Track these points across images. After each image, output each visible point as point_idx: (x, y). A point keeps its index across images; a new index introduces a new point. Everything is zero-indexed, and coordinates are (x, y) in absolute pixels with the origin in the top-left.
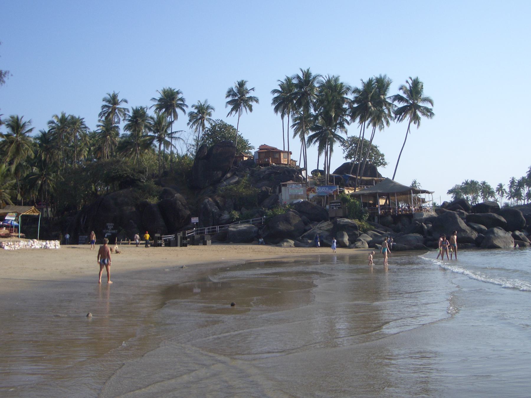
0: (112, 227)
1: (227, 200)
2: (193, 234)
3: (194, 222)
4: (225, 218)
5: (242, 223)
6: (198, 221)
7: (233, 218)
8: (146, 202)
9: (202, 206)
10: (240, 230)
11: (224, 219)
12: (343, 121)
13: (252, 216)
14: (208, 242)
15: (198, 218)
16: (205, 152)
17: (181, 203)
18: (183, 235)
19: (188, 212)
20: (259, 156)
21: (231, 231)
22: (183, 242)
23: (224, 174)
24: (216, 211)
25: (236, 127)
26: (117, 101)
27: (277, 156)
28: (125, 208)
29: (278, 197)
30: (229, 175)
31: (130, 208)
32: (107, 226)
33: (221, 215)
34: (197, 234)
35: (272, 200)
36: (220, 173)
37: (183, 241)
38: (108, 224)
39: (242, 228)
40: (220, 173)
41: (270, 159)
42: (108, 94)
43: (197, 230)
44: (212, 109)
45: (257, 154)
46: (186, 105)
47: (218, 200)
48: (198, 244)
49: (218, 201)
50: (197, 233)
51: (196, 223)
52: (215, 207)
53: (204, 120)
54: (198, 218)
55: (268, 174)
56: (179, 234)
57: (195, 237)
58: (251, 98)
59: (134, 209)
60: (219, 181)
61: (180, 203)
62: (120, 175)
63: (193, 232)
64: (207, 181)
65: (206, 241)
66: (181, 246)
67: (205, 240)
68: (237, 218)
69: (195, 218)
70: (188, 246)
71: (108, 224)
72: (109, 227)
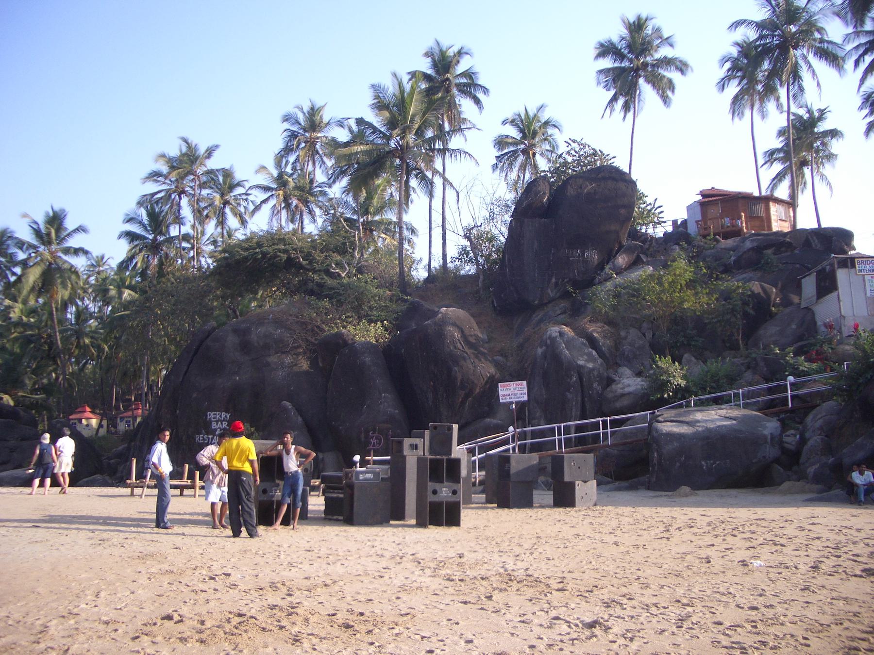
0: (225, 425)
1: (623, 334)
2: (507, 450)
3: (508, 400)
4: (627, 390)
5: (702, 404)
6: (526, 398)
7: (662, 386)
8: (339, 335)
9: (540, 351)
10: (708, 430)
11: (623, 395)
12: (604, 388)
13: (732, 380)
14: (579, 487)
15: (525, 383)
16: (544, 194)
17: (464, 336)
18: (432, 451)
19: (486, 369)
20: (704, 214)
21: (671, 436)
22: (431, 498)
23: (609, 256)
24: (590, 365)
25: (622, 164)
26: (317, 122)
27: (760, 209)
28: (273, 359)
29: (813, 314)
30: (622, 260)
31: (288, 360)
32: (210, 422)
33: (610, 381)
34: (523, 449)
35: (794, 326)
36: (593, 256)
37: (431, 486)
38: (211, 415)
39: (712, 421)
40: (593, 256)
41: (740, 218)
42: (298, 107)
43: (523, 436)
44: (555, 126)
45: (698, 209)
46: (480, 85)
47: (595, 330)
48: (526, 502)
49: (595, 335)
50: (520, 446)
51: (517, 403)
52: (586, 351)
53: (534, 154)
54: (525, 383)
55: (752, 249)
56: (415, 447)
57: (513, 463)
58: (667, 62)
59: (305, 365)
60: (587, 282)
61: (457, 335)
62: (264, 254)
63: (505, 442)
64: (554, 280)
65: (571, 486)
66: (421, 524)
67: (567, 479)
68: (678, 390)
69: (512, 384)
70: (467, 515)
71: (211, 415)
72: (214, 425)
